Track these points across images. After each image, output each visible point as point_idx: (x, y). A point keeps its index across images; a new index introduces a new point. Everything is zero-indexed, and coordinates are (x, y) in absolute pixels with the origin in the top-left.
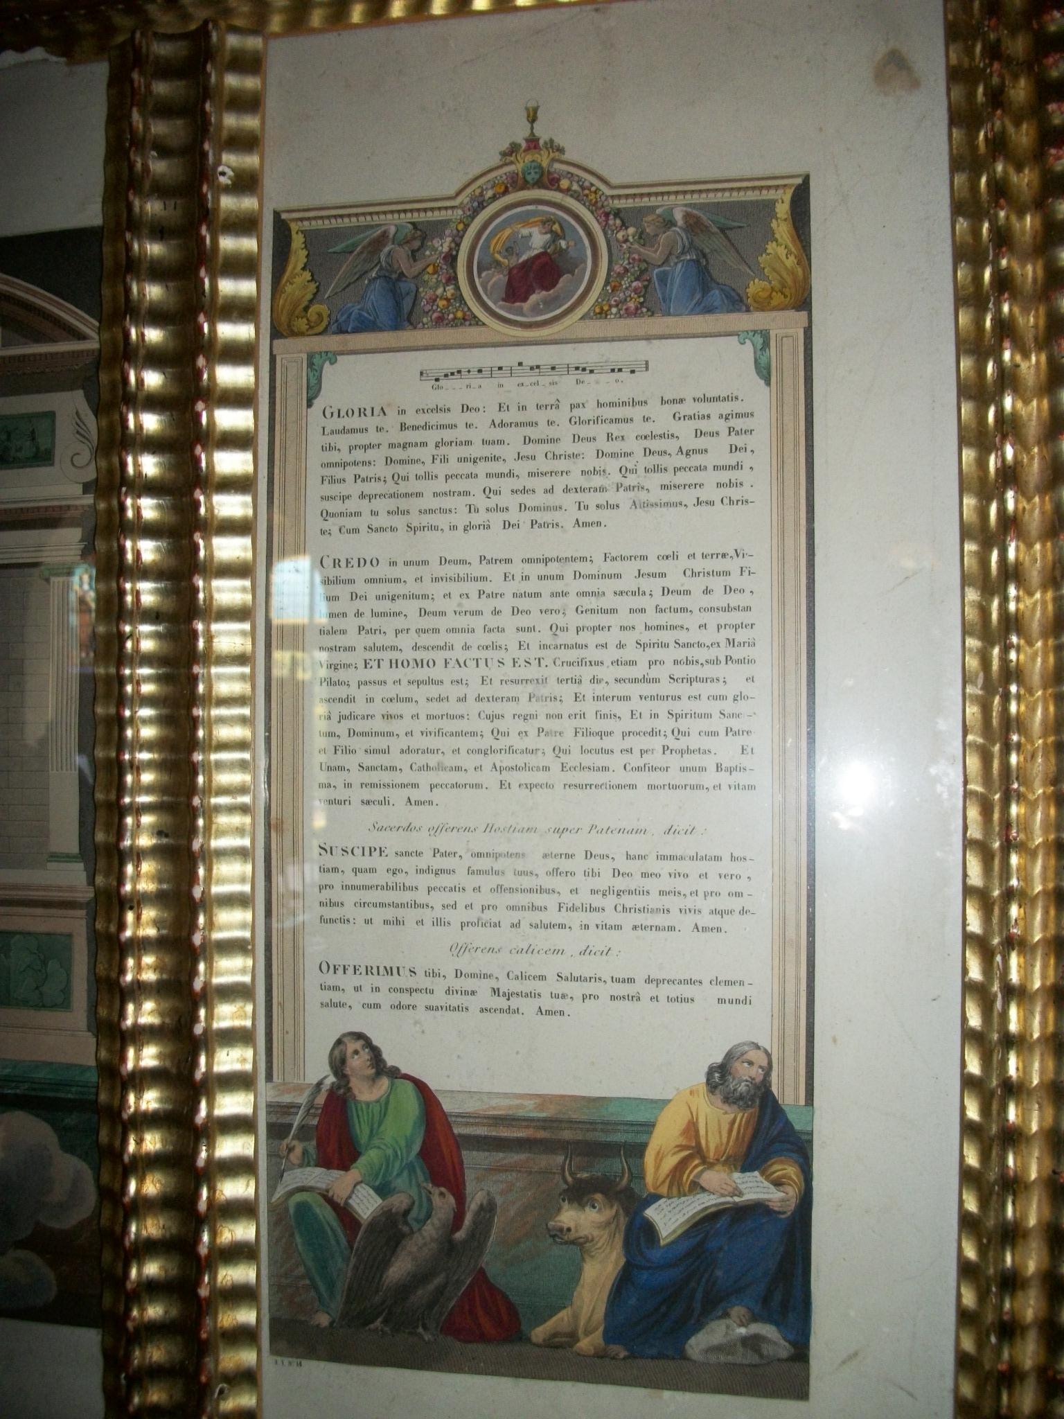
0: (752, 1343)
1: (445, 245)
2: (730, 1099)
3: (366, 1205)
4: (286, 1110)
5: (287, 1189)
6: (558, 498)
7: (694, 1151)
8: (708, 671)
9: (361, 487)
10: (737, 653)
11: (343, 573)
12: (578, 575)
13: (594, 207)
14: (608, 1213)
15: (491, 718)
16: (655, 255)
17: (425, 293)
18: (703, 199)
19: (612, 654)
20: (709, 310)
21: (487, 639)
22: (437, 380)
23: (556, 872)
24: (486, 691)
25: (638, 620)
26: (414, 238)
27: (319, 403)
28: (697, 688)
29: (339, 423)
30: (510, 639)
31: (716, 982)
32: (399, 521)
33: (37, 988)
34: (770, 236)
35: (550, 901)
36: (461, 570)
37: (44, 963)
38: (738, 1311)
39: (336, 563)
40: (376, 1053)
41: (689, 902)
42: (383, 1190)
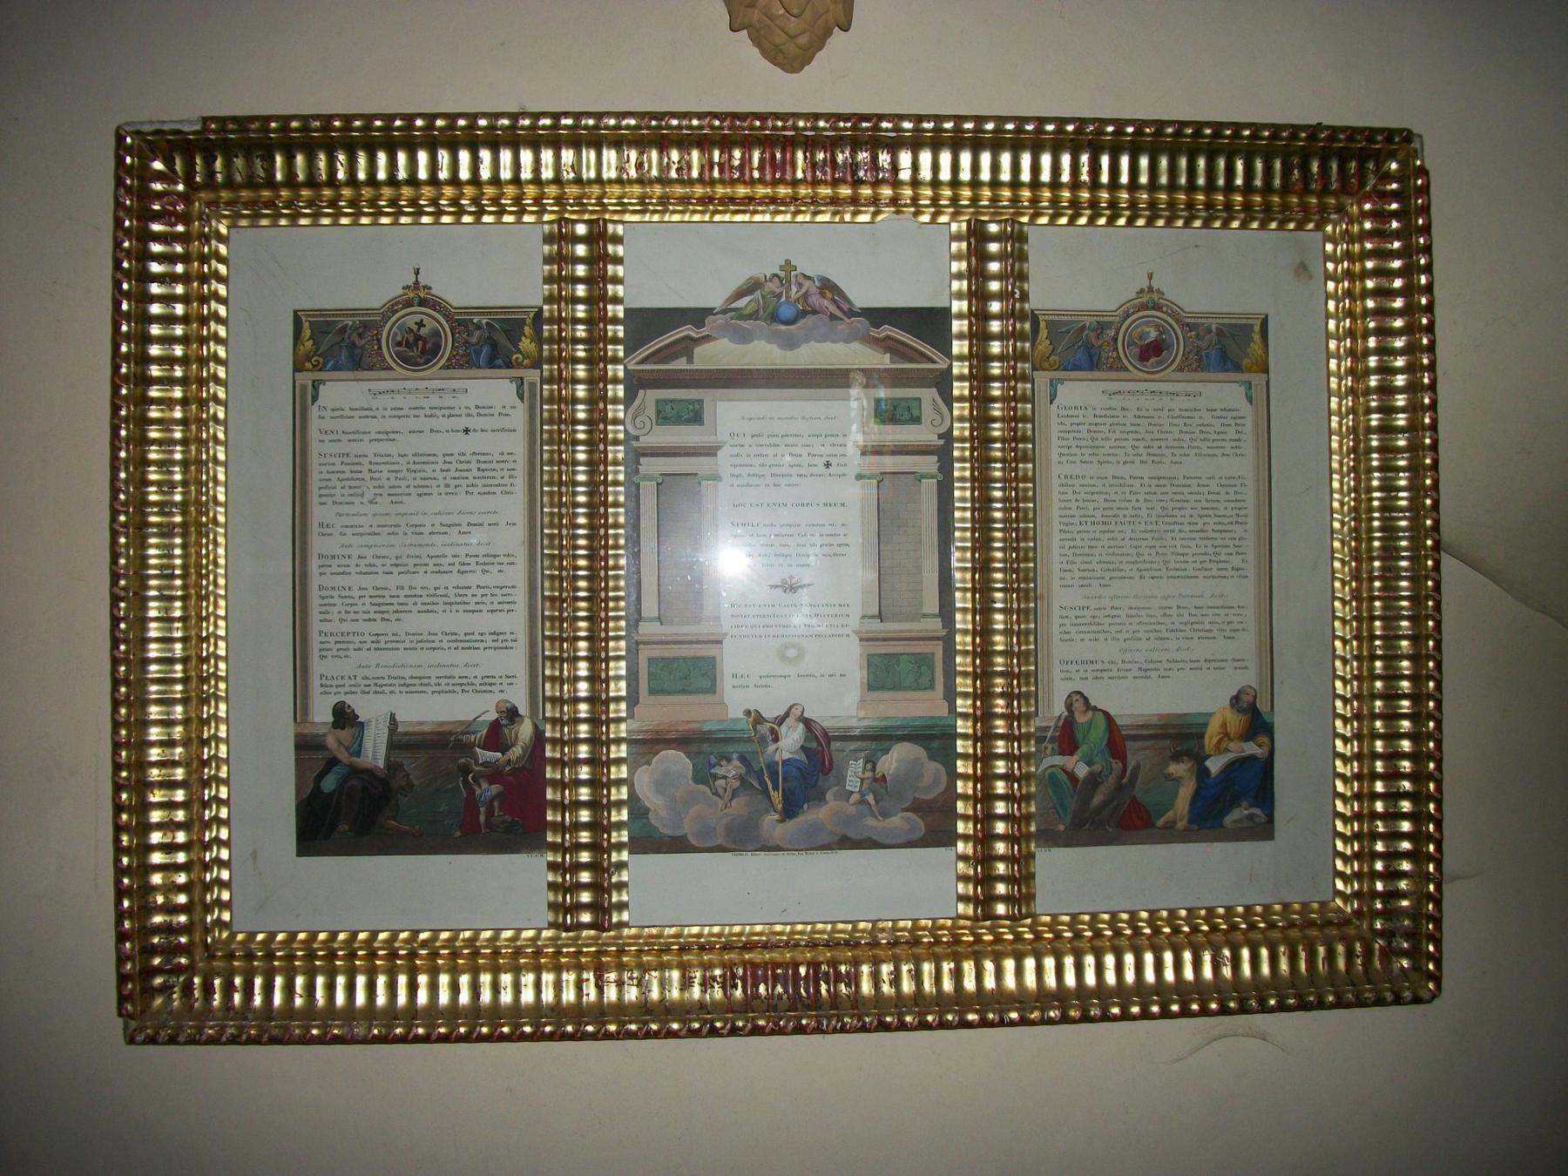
0: (1250, 817)
1: (1112, 333)
2: (1240, 711)
3: (1082, 771)
6: (1163, 451)
7: (1225, 735)
8: (1229, 527)
9: (1078, 443)
10: (1240, 520)
11: (1069, 482)
12: (1172, 485)
13: (1177, 321)
14: (1189, 765)
15: (1136, 547)
16: (1204, 344)
17: (1104, 355)
18: (1227, 321)
19: (1188, 519)
20: (1227, 371)
21: (1133, 512)
23: (1165, 615)
24: (1133, 536)
25: (1199, 505)
28: (1224, 535)
29: (1064, 412)
30: (1144, 512)
31: (1234, 660)
32: (1094, 459)
34: (1252, 340)
35: (1163, 628)
36: (1122, 481)
38: (1245, 803)
39: (1066, 477)
40: (1086, 699)
41: (1222, 626)
42: (1089, 764)
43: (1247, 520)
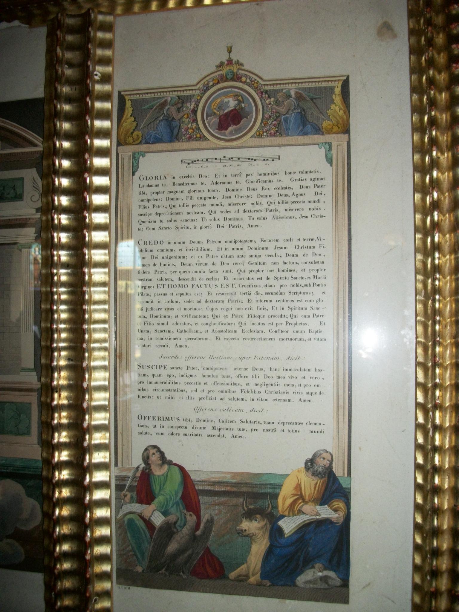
0: (325, 579)
1: (192, 106)
2: (315, 474)
3: (158, 520)
4: (123, 479)
5: (124, 513)
6: (241, 215)
7: (299, 496)
8: (306, 289)
9: (156, 210)
10: (318, 282)
11: (148, 247)
12: (249, 248)
13: (256, 89)
14: (262, 523)
15: (212, 309)
16: (283, 110)
17: (183, 126)
18: (303, 86)
19: (264, 282)
20: (306, 134)
21: (210, 276)
22: (189, 164)
23: (240, 376)
24: (209, 298)
25: (275, 267)
26: (179, 103)
27: (137, 174)
28: (301, 297)
29: (146, 183)
30: (220, 275)
31: (309, 423)
32: (172, 225)
33: (16, 426)
34: (332, 102)
35: (237, 389)
36: (199, 246)
37: (19, 415)
38: (318, 565)
39: (145, 243)
40: (162, 454)
41: (297, 389)
42: (165, 513)
43: (139, 335)
